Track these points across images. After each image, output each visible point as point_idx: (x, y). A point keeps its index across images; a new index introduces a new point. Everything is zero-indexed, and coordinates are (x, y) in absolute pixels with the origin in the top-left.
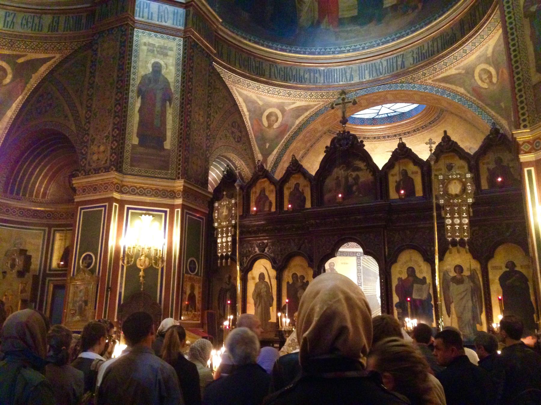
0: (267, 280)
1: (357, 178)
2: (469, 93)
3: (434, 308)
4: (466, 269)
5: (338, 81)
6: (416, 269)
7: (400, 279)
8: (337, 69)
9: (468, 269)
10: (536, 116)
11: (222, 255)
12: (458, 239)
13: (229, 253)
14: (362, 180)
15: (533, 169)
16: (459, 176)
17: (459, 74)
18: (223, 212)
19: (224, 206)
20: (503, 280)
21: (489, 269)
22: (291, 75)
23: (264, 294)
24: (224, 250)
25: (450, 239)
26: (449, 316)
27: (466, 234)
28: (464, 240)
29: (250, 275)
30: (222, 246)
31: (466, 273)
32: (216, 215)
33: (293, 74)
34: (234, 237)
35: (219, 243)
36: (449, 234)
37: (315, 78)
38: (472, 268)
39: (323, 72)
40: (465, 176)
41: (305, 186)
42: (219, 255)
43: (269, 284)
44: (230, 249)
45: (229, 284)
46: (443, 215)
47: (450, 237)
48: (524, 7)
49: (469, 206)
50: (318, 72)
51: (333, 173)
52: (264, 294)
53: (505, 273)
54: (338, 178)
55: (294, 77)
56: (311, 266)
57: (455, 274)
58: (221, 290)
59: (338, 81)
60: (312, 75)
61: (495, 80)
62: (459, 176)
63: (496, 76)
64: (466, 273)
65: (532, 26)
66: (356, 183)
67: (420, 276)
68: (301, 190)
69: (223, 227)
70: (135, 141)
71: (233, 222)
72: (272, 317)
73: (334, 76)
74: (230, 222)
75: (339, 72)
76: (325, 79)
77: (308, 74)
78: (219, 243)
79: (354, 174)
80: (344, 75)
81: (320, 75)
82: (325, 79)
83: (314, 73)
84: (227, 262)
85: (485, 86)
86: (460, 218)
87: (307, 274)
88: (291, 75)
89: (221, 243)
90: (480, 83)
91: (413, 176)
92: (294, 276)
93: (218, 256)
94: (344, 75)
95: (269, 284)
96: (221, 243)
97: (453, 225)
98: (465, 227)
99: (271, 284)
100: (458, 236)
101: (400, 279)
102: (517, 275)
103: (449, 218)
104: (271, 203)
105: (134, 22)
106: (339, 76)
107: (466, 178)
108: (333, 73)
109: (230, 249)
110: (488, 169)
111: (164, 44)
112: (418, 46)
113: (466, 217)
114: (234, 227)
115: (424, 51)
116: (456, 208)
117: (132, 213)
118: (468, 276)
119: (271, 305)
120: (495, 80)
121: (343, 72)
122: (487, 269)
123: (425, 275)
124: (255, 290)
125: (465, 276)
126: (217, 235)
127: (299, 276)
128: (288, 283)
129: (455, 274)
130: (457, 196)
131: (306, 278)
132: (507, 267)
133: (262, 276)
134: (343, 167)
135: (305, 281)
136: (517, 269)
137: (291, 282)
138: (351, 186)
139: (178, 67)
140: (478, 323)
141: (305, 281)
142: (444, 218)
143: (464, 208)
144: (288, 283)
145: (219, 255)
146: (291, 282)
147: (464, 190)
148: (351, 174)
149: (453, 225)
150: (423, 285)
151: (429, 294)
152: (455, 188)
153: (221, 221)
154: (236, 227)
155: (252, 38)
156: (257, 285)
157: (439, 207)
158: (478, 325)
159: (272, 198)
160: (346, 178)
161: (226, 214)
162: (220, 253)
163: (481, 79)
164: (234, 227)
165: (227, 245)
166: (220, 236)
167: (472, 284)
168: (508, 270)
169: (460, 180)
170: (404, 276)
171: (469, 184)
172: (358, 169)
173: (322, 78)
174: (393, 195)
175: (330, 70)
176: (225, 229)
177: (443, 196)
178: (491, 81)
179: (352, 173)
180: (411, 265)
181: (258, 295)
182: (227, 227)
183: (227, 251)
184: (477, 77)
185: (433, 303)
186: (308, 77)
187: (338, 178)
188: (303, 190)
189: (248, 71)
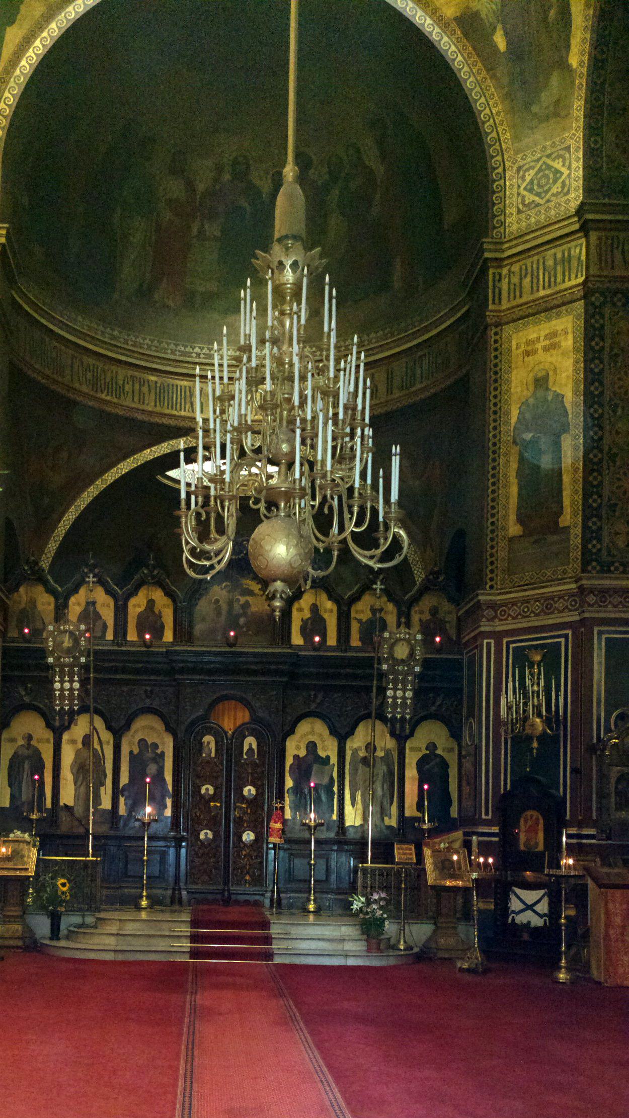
1: (247, 605)
3: (336, 796)
5: (178, 408)
7: (296, 757)
8: (177, 386)
10: (506, 577)
11: (62, 709)
12: (399, 716)
14: (253, 609)
16: (407, 636)
18: (63, 642)
19: (66, 632)
20: (421, 764)
21: (407, 751)
22: (103, 382)
26: (353, 807)
31: (380, 754)
33: (107, 381)
35: (56, 690)
36: (389, 710)
37: (142, 395)
39: (154, 385)
40: (415, 636)
41: (165, 606)
42: (58, 708)
44: (76, 702)
46: (384, 685)
47: (390, 713)
49: (416, 676)
50: (146, 383)
51: (210, 594)
53: (424, 756)
54: (217, 601)
55: (108, 386)
59: (178, 408)
60: (137, 386)
62: (407, 636)
64: (380, 754)
66: (245, 614)
67: (322, 754)
68: (157, 612)
70: (514, 529)
71: (83, 660)
72: (103, 803)
73: (173, 398)
74: (76, 659)
75: (181, 390)
76: (158, 400)
77: (131, 383)
78: (56, 690)
79: (243, 600)
80: (188, 400)
81: (150, 391)
82: (158, 400)
83: (140, 385)
86: (404, 690)
87: (163, 743)
88: (103, 382)
89: (59, 690)
91: (326, 616)
93: (55, 710)
94: (188, 400)
95: (100, 753)
97: (395, 698)
100: (399, 713)
101: (296, 757)
102: (438, 759)
103: (391, 689)
104: (105, 627)
106: (181, 399)
108: (171, 394)
110: (420, 620)
111: (449, 622)
113: (410, 690)
114: (86, 667)
116: (400, 677)
119: (103, 784)
121: (188, 393)
122: (404, 748)
123: (329, 753)
124: (75, 761)
127: (149, 743)
130: (403, 661)
131: (160, 747)
132: (427, 749)
134: (226, 586)
135: (159, 751)
137: (136, 751)
138: (238, 616)
140: (386, 816)
141: (159, 751)
142: (385, 689)
143: (410, 678)
144: (131, 753)
145: (58, 708)
146: (136, 751)
147: (412, 654)
148: (238, 599)
149: (395, 698)
151: (332, 779)
152: (401, 652)
155: (47, 300)
156: (78, 753)
157: (382, 675)
158: (386, 818)
159: (108, 614)
160: (230, 603)
168: (428, 752)
169: (408, 641)
170: (302, 753)
171: (418, 648)
172: (251, 593)
173: (153, 396)
174: (297, 640)
175: (166, 385)
177: (387, 660)
179: (240, 597)
180: (311, 738)
183: (71, 705)
185: (335, 789)
186: (131, 391)
187: (217, 601)
188: (160, 612)
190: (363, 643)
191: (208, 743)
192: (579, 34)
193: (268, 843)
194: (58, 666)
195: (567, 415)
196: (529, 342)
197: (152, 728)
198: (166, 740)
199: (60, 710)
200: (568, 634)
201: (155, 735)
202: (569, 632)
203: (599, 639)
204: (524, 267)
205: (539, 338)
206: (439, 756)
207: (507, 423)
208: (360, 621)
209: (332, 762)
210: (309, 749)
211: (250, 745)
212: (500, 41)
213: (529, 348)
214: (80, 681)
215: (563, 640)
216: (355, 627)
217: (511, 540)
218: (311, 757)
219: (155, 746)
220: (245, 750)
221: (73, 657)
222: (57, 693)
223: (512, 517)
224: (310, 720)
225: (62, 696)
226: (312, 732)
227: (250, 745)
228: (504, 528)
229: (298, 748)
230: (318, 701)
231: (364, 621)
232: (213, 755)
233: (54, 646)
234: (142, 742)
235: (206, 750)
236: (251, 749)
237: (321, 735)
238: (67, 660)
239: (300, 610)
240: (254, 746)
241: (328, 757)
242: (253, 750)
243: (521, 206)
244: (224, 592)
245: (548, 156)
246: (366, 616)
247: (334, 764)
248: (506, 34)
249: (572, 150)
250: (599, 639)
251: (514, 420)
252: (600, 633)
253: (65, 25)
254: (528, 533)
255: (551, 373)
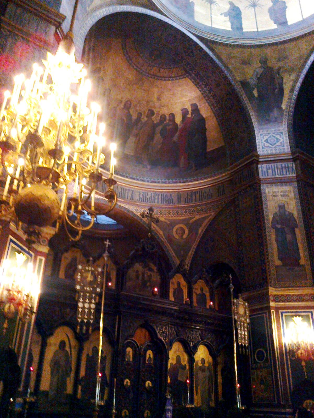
0: (67, 348)
1: (150, 276)
2: (164, 235)
11: (83, 321)
13: (92, 321)
15: (43, 259)
17: (166, 223)
18: (87, 277)
19: (89, 271)
23: (62, 363)
24: (86, 317)
28: (90, 322)
30: (83, 312)
32: (79, 277)
34: (98, 305)
41: (112, 269)
42: (79, 320)
43: (69, 353)
47: (80, 318)
48: (272, 223)
52: (62, 363)
61: (185, 236)
63: (187, 235)
65: (277, 235)
66: (149, 280)
69: (86, 292)
70: (278, 262)
71: (98, 290)
74: (95, 289)
79: (149, 273)
84: (87, 330)
85: (177, 237)
90: (175, 234)
91: (182, 288)
93: (78, 321)
95: (69, 353)
96: (82, 308)
98: (92, 311)
99: (71, 354)
101: (171, 364)
105: (259, 180)
107: (80, 285)
109: (247, 342)
112: (144, 191)
114: (100, 295)
115: (148, 197)
117: (285, 316)
119: (68, 375)
120: (185, 236)
126: (79, 298)
133: (62, 344)
137: (91, 355)
139: (267, 217)
144: (88, 355)
146: (91, 355)
153: (84, 286)
154: (102, 296)
156: (56, 353)
161: (92, 280)
163: (176, 232)
164: (100, 295)
165: (89, 313)
166: (81, 300)
172: (151, 270)
176: (88, 295)
178: (182, 236)
181: (55, 364)
182: (91, 293)
183: (89, 319)
184: (174, 230)
187: (137, 271)
189: (180, 194)
190: (198, 305)
191: (129, 352)
192: (286, 99)
194: (83, 292)
195: (296, 222)
196: (275, 192)
199: (81, 322)
200: (281, 312)
202: (280, 311)
203: (282, 316)
204: (268, 166)
205: (278, 192)
207: (268, 220)
208: (196, 294)
211: (150, 355)
212: (255, 93)
213: (274, 194)
214: (96, 304)
215: (265, 315)
216: (195, 296)
217: (277, 267)
220: (147, 359)
221: (92, 288)
222: (80, 310)
223: (276, 257)
225: (83, 312)
227: (150, 355)
228: (273, 261)
231: (198, 294)
232: (131, 360)
233: (81, 279)
235: (128, 356)
236: (150, 357)
238: (88, 289)
239: (173, 283)
240: (152, 356)
242: (151, 358)
243: (263, 146)
244: (141, 268)
245: (274, 133)
246: (199, 292)
248: (258, 91)
249: (283, 134)
250: (282, 316)
251: (161, 233)
252: (282, 313)
253: (115, 11)
254: (284, 265)
255: (286, 205)
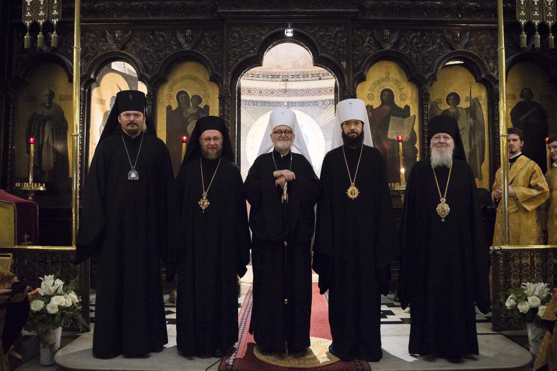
4: (464, 99)
6: (394, 93)
9: (467, 98)
11: (35, 25)
25: (523, 22)
27: (550, 14)
29: (95, 93)
31: (464, 104)
38: (473, 97)
44: (55, 12)
45: (49, 108)
47: (523, 18)
56: (214, 79)
57: (448, 107)
58: (32, 117)
64: (464, 104)
67: (399, 103)
87: (207, 96)
92: (183, 95)
118: (466, 109)
123: (408, 102)
125: (461, 108)
127: (191, 97)
128: (169, 108)
129: (448, 107)
131: (204, 100)
135: (202, 106)
136: (533, 100)
137: (175, 106)
141: (202, 106)
144: (169, 108)
145: (28, 23)
150: (405, 118)
151: (413, 133)
162: (28, 19)
167: (471, 120)
168: (523, 100)
183: (49, 16)
193: (287, 196)
197: (195, 79)
198: (210, 91)
201: (198, 86)
206: (535, 104)
209: (412, 113)
210: (385, 98)
218: (387, 108)
219: (198, 99)
224: (385, 64)
226: (387, 79)
229: (371, 97)
230: (393, 41)
234: (182, 95)
237: (397, 82)
241: (407, 108)
247: (415, 116)
